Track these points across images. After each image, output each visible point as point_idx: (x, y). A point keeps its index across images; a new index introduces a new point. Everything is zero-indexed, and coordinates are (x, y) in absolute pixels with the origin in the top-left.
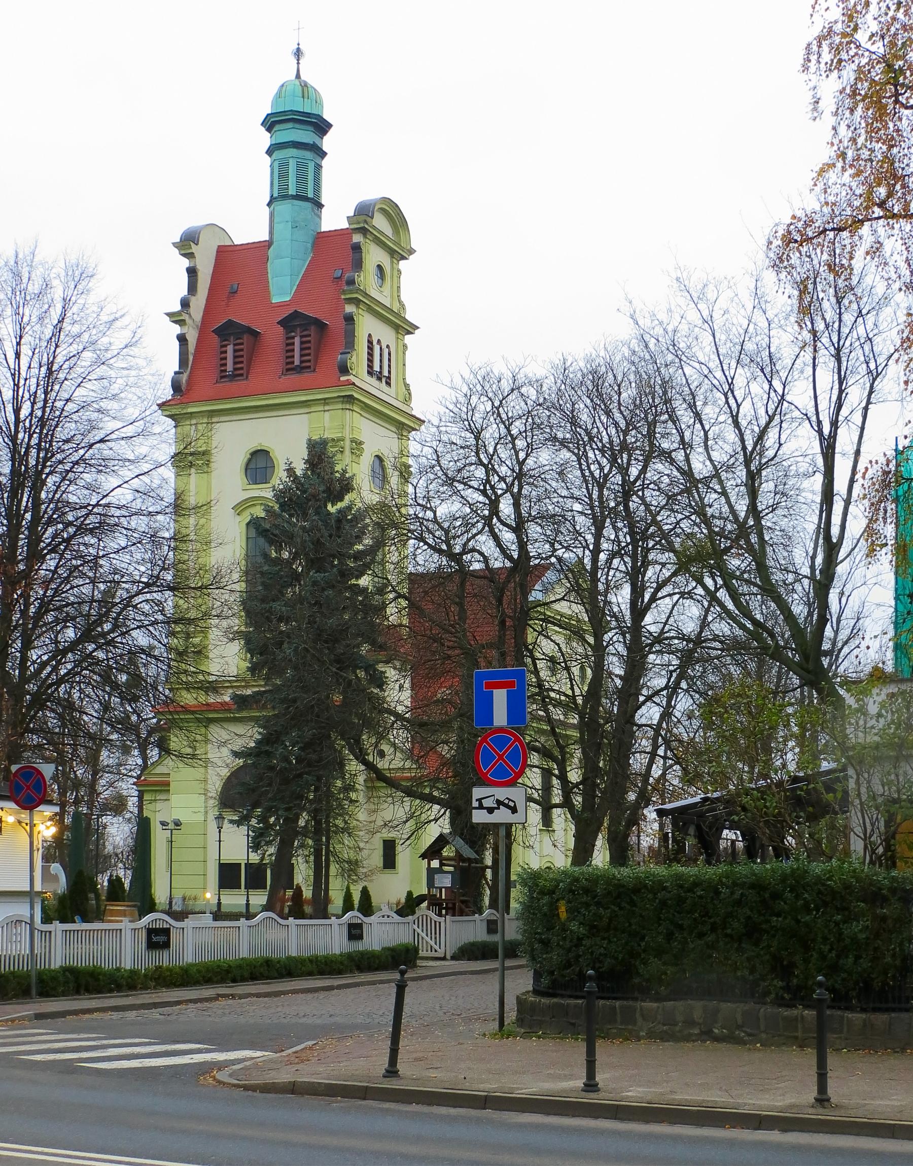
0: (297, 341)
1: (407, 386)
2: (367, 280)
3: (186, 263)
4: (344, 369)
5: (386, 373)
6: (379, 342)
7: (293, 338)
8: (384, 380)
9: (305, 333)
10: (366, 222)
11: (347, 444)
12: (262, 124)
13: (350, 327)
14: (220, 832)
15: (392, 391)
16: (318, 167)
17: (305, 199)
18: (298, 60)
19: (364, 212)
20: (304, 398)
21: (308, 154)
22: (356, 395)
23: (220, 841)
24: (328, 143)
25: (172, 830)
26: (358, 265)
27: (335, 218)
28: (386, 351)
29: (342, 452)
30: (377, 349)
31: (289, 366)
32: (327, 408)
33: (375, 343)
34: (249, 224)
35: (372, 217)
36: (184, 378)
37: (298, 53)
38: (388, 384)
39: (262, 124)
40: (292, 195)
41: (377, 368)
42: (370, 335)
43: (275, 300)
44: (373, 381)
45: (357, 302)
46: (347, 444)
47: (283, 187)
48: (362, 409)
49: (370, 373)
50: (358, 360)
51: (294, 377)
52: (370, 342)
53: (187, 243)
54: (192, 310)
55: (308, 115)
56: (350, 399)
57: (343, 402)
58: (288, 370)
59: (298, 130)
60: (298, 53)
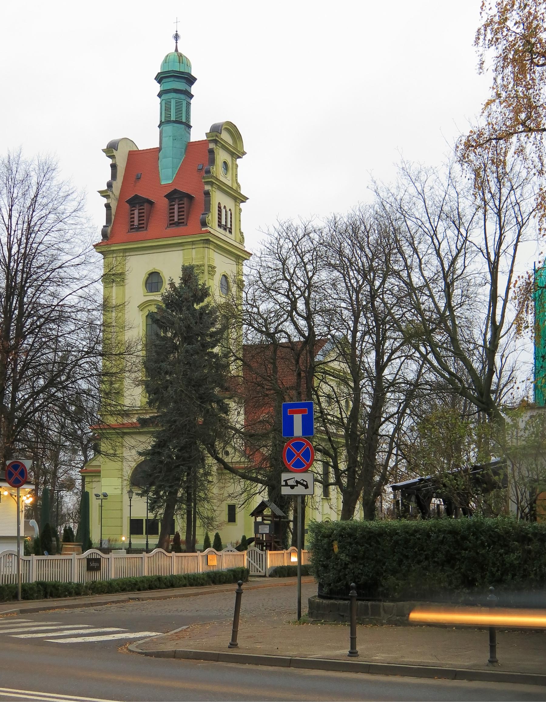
0: (176, 207)
3: (110, 161)
4: (204, 224)
5: (229, 226)
6: (225, 207)
7: (174, 205)
9: (181, 202)
10: (217, 136)
11: (206, 268)
12: (155, 79)
13: (207, 198)
14: (130, 500)
16: (189, 104)
17: (181, 123)
19: (216, 130)
20: (180, 241)
21: (182, 96)
22: (211, 239)
23: (130, 506)
24: (194, 89)
25: (102, 499)
28: (229, 213)
29: (203, 273)
31: (171, 222)
32: (194, 247)
33: (222, 208)
34: (147, 138)
35: (221, 134)
36: (109, 229)
37: (176, 37)
38: (230, 232)
41: (223, 223)
42: (219, 203)
43: (163, 183)
44: (221, 230)
45: (211, 184)
47: (168, 115)
48: (215, 247)
50: (213, 218)
51: (174, 229)
52: (219, 207)
53: (111, 149)
54: (114, 189)
55: (183, 73)
56: (207, 241)
58: (171, 224)
59: (176, 81)
60: (176, 37)
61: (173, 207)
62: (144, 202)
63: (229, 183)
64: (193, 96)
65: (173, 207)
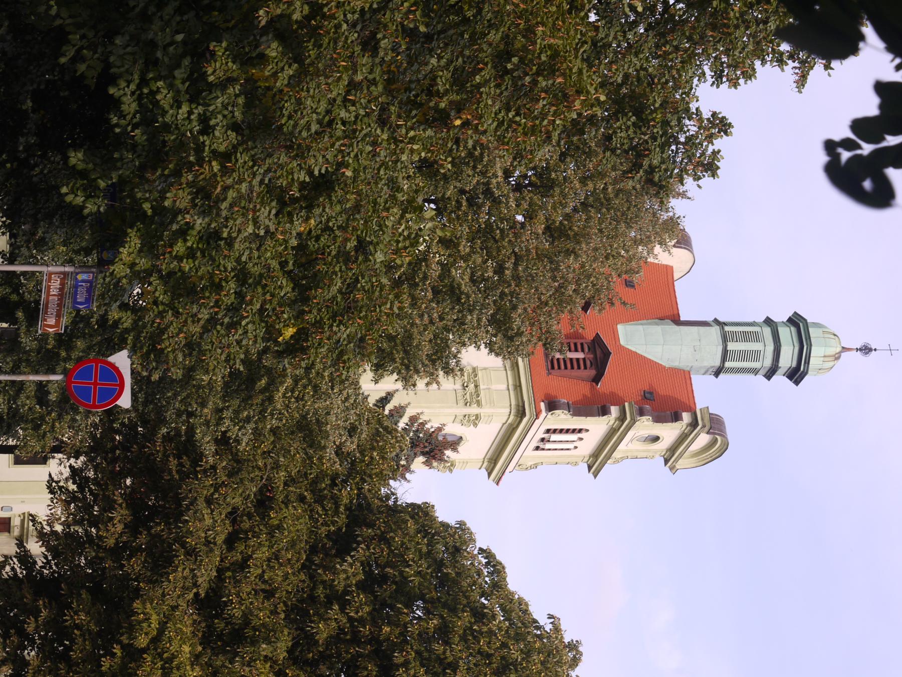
0: (580, 355)
1: (535, 466)
2: (645, 426)
4: (552, 406)
5: (548, 446)
6: (581, 439)
7: (583, 350)
8: (546, 436)
9: (588, 363)
10: (704, 426)
12: (795, 313)
15: (530, 452)
16: (755, 372)
17: (724, 359)
18: (861, 350)
19: (716, 425)
22: (525, 420)
26: (658, 419)
27: (707, 393)
28: (571, 446)
30: (574, 437)
33: (580, 435)
35: (708, 433)
37: (866, 350)
38: (537, 448)
39: (795, 313)
40: (726, 346)
41: (554, 437)
42: (587, 431)
43: (621, 328)
44: (541, 434)
45: (622, 418)
46: (473, 410)
48: (511, 425)
49: (548, 431)
50: (562, 419)
52: (580, 431)
55: (807, 362)
56: (521, 413)
57: (518, 406)
60: (866, 350)
61: (579, 349)
62: (597, 369)
63: (622, 446)
64: (769, 379)
65: (579, 349)
